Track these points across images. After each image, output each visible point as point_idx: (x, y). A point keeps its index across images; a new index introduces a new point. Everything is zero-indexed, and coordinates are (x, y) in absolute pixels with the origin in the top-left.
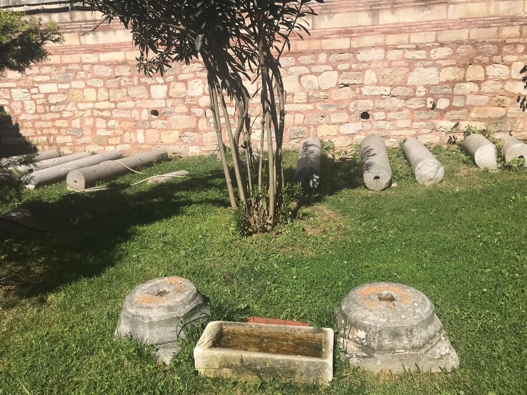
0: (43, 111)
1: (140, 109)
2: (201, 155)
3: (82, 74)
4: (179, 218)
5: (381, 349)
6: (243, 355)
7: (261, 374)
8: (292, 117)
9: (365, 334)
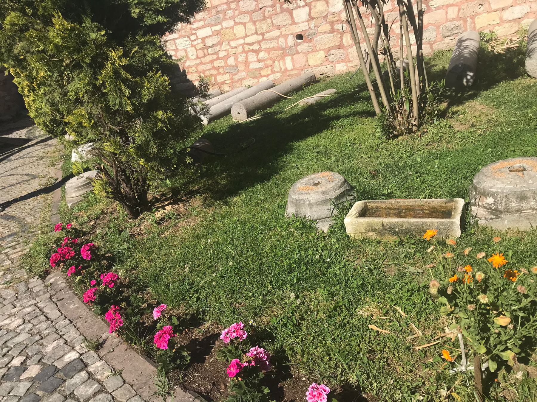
0: (203, 55)
1: (286, 36)
2: (348, 71)
3: (230, 13)
4: (329, 131)
5: (508, 211)
6: (384, 221)
7: (400, 235)
8: (444, 12)
9: (494, 200)
